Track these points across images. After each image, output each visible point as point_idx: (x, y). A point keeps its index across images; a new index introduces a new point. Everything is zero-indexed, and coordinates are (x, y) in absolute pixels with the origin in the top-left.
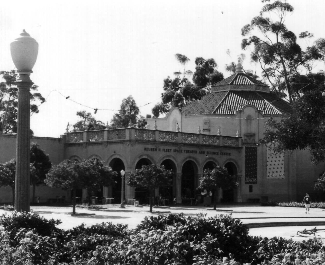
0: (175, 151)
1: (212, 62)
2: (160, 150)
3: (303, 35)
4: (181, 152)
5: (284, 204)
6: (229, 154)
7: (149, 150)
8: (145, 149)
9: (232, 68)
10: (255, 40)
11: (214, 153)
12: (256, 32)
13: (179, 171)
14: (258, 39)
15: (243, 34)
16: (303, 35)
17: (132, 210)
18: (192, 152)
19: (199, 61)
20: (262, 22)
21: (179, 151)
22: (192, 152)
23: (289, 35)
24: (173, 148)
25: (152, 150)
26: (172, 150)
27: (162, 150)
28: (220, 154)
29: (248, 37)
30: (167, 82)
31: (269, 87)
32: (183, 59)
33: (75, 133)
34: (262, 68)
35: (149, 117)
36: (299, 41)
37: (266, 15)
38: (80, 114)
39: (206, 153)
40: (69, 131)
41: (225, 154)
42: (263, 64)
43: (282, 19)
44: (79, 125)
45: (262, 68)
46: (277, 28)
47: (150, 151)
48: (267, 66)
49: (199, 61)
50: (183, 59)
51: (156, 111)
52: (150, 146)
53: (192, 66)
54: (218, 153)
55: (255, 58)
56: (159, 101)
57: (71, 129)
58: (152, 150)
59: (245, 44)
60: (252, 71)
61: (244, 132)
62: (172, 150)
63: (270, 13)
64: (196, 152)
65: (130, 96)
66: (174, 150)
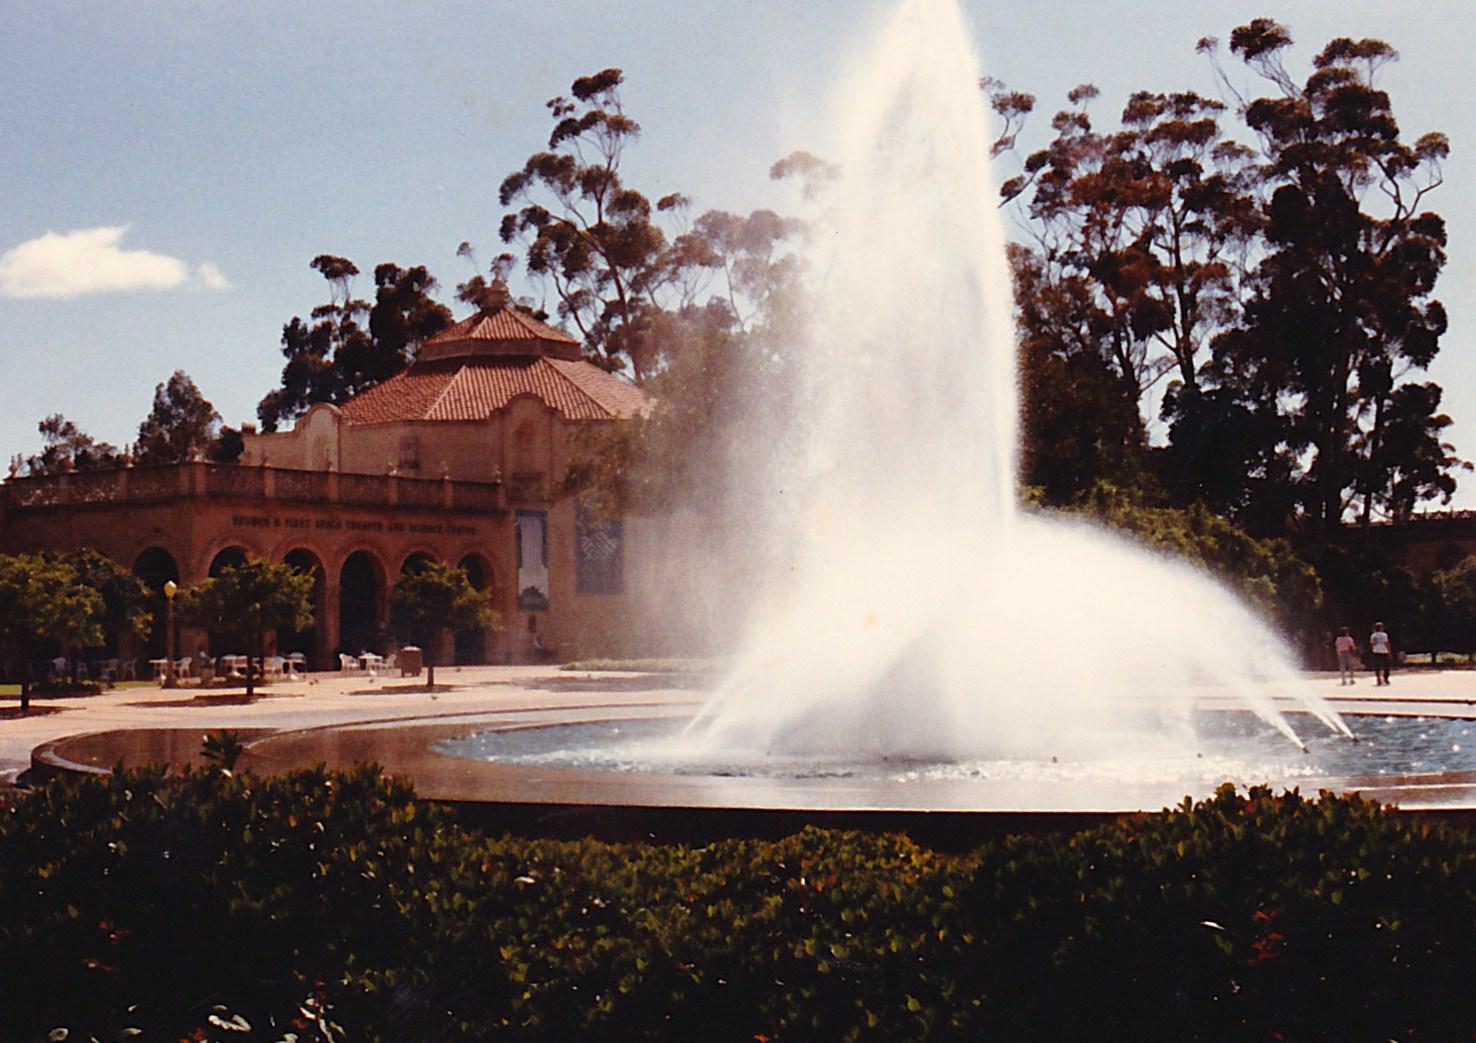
0: (320, 525)
1: (419, 275)
2: (277, 523)
3: (667, 203)
4: (402, 530)
5: (1419, 658)
6: (473, 531)
7: (248, 523)
8: (238, 521)
9: (474, 291)
10: (536, 216)
11: (431, 529)
12: (540, 194)
13: (333, 580)
14: (547, 213)
15: (505, 200)
16: (667, 203)
17: (353, 697)
18: (367, 526)
19: (384, 272)
20: (549, 168)
21: (331, 525)
22: (367, 526)
23: (629, 201)
24: (313, 517)
25: (255, 522)
26: (313, 524)
27: (283, 522)
28: (390, 529)
29: (517, 206)
30: (293, 334)
31: (579, 344)
32: (334, 268)
33: (36, 478)
34: (560, 292)
35: (249, 430)
36: (657, 219)
37: (564, 149)
38: (48, 427)
39: (407, 528)
40: (18, 474)
41: (459, 531)
42: (563, 281)
43: (611, 158)
44: (50, 453)
45: (560, 292)
46: (596, 181)
47: (250, 527)
48: (574, 288)
49: (384, 272)
50: (334, 268)
51: (271, 409)
52: (248, 512)
53: (364, 289)
54: (441, 528)
55: (537, 263)
56: (272, 380)
57: (25, 471)
58: (255, 522)
59: (507, 230)
60: (532, 299)
61: (510, 465)
62: (313, 524)
63: (576, 144)
64: (380, 527)
65: (176, 374)
66: (317, 523)
